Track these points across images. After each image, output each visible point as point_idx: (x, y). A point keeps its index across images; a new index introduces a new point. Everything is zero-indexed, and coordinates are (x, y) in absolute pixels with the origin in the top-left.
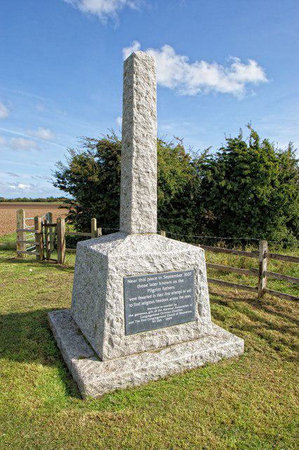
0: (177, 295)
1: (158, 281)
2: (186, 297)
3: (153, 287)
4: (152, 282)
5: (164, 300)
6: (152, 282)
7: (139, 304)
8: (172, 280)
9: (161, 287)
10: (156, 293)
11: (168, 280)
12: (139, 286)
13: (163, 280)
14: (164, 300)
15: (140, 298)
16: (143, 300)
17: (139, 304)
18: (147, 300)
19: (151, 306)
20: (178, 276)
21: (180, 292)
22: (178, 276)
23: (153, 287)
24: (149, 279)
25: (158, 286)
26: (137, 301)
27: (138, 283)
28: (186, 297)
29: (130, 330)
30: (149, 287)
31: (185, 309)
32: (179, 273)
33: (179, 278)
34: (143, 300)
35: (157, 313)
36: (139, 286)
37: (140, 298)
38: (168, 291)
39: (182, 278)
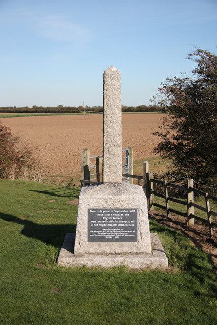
0: (124, 224)
1: (110, 213)
2: (130, 225)
3: (107, 217)
4: (106, 213)
5: (114, 225)
6: (106, 213)
7: (97, 225)
8: (121, 213)
9: (112, 217)
10: (109, 220)
11: (116, 213)
12: (97, 215)
13: (114, 213)
14: (114, 225)
15: (98, 222)
16: (100, 224)
17: (97, 225)
18: (102, 223)
19: (104, 227)
20: (124, 211)
21: (126, 222)
22: (124, 211)
23: (107, 217)
24: (104, 211)
25: (110, 216)
26: (96, 223)
27: (97, 213)
28: (130, 225)
29: (91, 239)
30: (104, 216)
31: (129, 233)
32: (126, 210)
33: (126, 213)
34: (100, 224)
35: (109, 232)
36: (97, 215)
37: (98, 222)
38: (118, 220)
39: (127, 213)
